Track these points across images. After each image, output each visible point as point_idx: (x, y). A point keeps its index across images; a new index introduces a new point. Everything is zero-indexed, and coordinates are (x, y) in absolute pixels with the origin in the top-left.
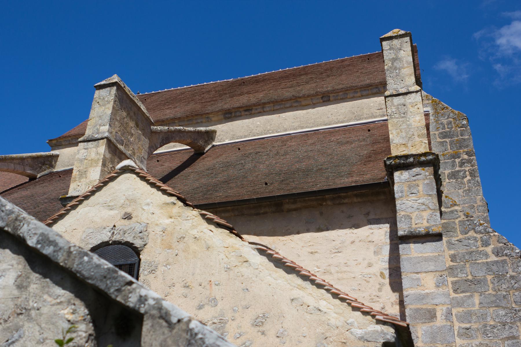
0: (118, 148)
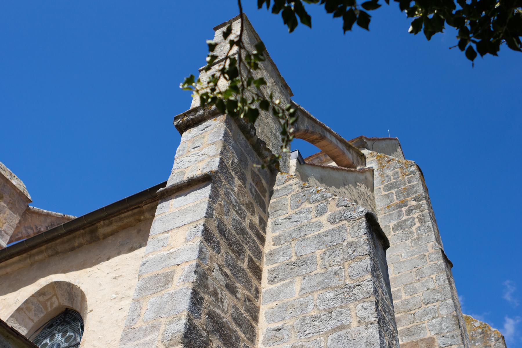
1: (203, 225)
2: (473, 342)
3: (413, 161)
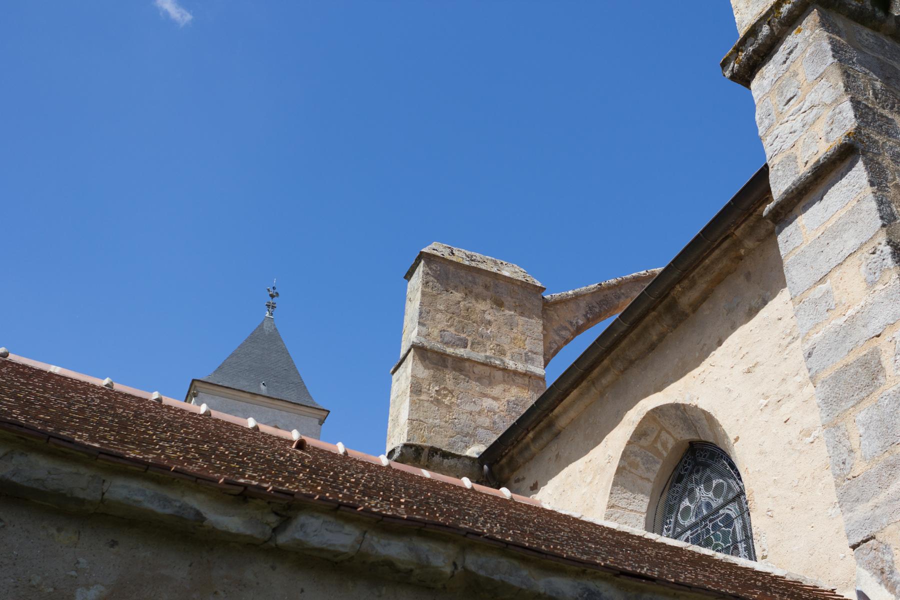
0: (448, 355)
1: (888, 243)
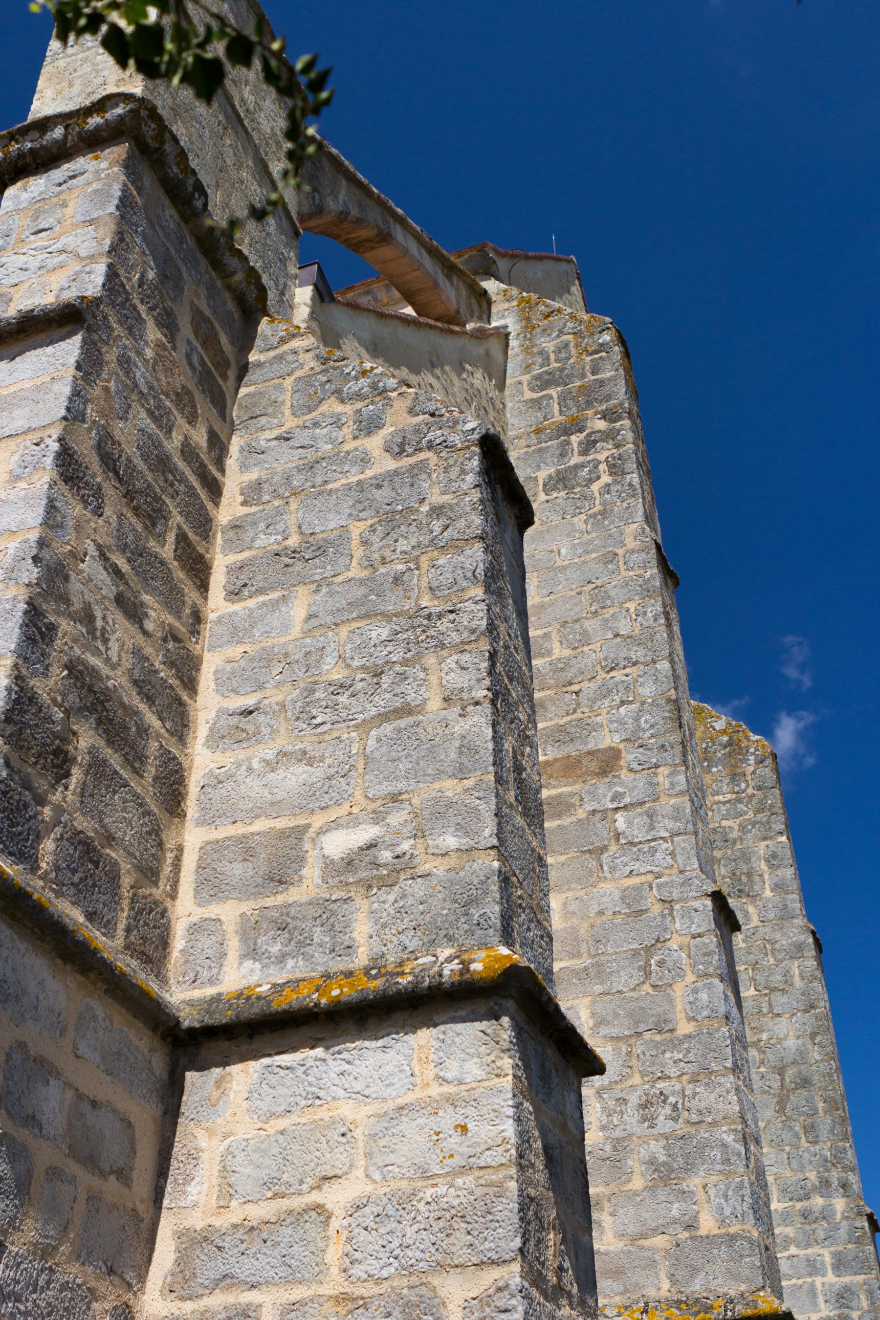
1: (60, 440)
2: (706, 764)
3: (608, 320)
